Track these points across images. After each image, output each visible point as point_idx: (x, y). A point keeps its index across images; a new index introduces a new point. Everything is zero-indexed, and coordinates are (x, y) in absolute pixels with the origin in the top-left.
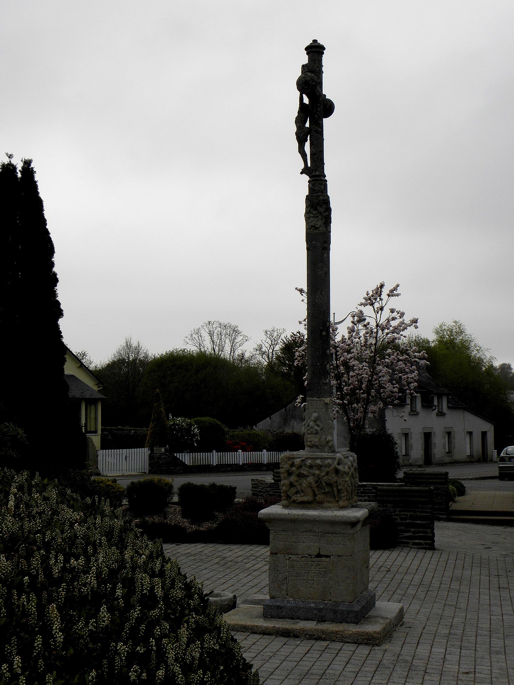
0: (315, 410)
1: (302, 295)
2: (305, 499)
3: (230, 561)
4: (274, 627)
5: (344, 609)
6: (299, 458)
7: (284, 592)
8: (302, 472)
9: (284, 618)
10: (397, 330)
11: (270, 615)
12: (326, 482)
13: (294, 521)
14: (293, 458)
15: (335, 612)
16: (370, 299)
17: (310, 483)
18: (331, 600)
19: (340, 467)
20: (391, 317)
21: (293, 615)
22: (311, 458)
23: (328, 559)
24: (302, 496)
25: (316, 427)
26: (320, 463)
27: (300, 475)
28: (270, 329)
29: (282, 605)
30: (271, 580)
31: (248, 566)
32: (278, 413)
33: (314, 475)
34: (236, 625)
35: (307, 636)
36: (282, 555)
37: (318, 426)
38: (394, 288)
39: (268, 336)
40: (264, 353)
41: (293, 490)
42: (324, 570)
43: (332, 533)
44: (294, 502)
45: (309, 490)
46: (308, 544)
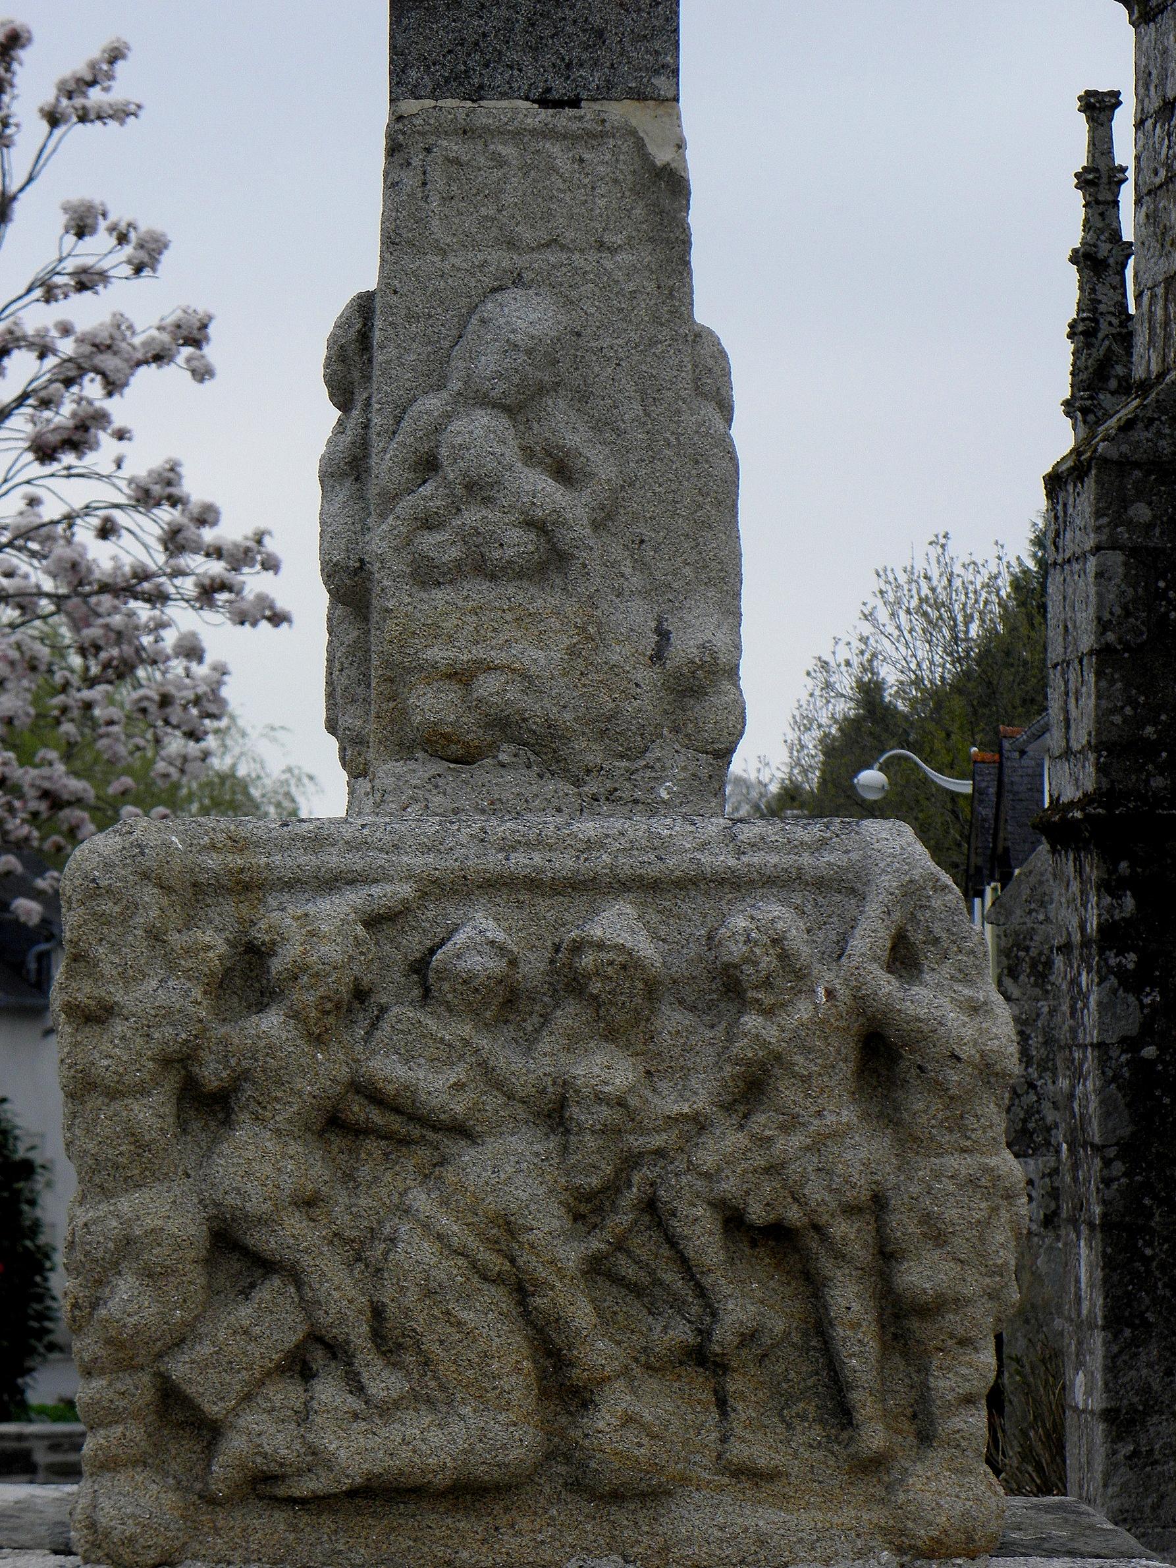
0: (501, 259)
2: (429, 1442)
6: (331, 883)
8: (389, 1069)
10: (108, 362)
12: (733, 1221)
14: (246, 887)
17: (507, 1229)
20: (70, 265)
22: (494, 885)
24: (386, 1410)
25: (538, 485)
26: (646, 948)
27: (358, 1122)
33: (554, 1112)
37: (564, 470)
38: (93, 66)
41: (264, 1322)
44: (263, 1486)
45: (490, 1324)
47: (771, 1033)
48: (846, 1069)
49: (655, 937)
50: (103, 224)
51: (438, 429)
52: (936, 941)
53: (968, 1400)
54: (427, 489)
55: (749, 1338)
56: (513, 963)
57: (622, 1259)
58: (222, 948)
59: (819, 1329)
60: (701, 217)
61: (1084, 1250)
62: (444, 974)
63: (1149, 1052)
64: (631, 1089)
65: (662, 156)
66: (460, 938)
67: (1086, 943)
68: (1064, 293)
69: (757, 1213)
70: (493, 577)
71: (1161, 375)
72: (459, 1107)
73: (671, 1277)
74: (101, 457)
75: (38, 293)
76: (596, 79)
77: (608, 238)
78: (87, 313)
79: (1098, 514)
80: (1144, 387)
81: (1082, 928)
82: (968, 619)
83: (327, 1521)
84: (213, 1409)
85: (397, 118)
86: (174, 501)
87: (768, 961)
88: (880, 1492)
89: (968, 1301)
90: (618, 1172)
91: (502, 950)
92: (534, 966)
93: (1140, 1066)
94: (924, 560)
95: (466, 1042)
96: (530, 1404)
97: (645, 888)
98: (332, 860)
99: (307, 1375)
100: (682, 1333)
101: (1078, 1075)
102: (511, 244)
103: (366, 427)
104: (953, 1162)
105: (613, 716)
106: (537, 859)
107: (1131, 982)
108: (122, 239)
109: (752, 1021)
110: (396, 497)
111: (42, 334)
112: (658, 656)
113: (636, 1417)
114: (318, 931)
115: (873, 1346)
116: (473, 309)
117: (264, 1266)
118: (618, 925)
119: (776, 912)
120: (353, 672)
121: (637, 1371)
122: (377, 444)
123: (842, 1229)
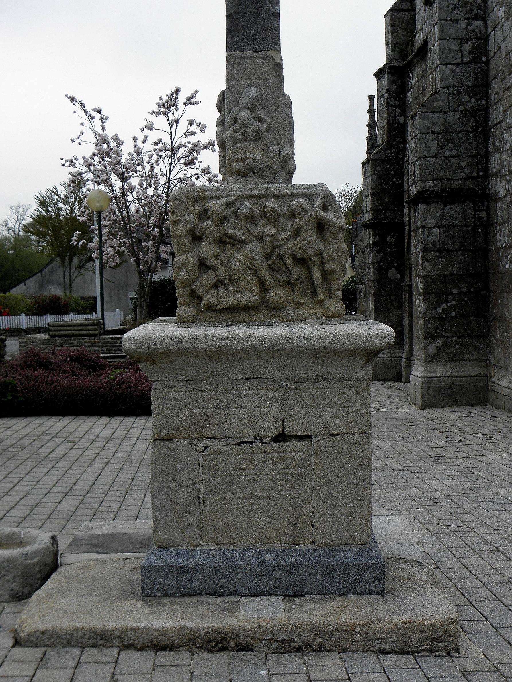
0: (248, 82)
1: (74, 104)
2: (240, 299)
3: (12, 446)
4: (183, 628)
5: (350, 562)
6: (219, 197)
7: (194, 532)
8: (231, 231)
9: (196, 594)
10: (197, 148)
11: (159, 590)
13: (219, 354)
15: (328, 571)
16: (164, 105)
17: (253, 260)
18: (314, 542)
19: (329, 216)
20: (189, 131)
21: (221, 587)
22: (249, 197)
23: (306, 444)
24: (232, 293)
25: (256, 124)
26: (277, 207)
27: (226, 242)
28: (15, 204)
29: (190, 564)
30: (158, 504)
31: (44, 451)
32: (33, 279)
33: (261, 238)
34: (77, 630)
35: (275, 645)
36: (187, 442)
37: (261, 121)
38: (192, 94)
39: (14, 211)
40: (10, 229)
41: (209, 278)
42: (294, 471)
43: (315, 381)
44: (210, 308)
45: (250, 277)
46: (254, 411)
47: (301, 222)
48: (315, 229)
49: (279, 206)
50: (195, 123)
51: (237, 114)
52: (331, 205)
53: (338, 289)
54: (236, 125)
55: (298, 279)
56: (253, 211)
57: (274, 265)
58: (199, 209)
59: (311, 277)
60: (286, 73)
61: (370, 299)
62: (240, 213)
63: (381, 264)
64: (275, 233)
65: (278, 61)
66: (243, 206)
67: (370, 245)
68: (365, 132)
69: (298, 256)
70: (248, 141)
71: (382, 144)
72: (244, 238)
73: (283, 268)
74: (196, 166)
75: (184, 136)
76: (265, 47)
77: (268, 77)
78: (193, 139)
79: (371, 169)
80: (379, 146)
81: (369, 242)
82: (352, 198)
83: (222, 314)
84: (201, 294)
85: (228, 55)
86: (209, 173)
87: (300, 209)
88: (322, 306)
89: (338, 271)
90: (273, 249)
91: (250, 208)
92: (257, 212)
93: (380, 267)
94: (344, 188)
95: (245, 226)
96: (258, 292)
97: (277, 197)
98: (219, 193)
99: (218, 288)
100: (286, 279)
101: (369, 269)
102: (250, 79)
103: (224, 115)
104: (334, 245)
105: (271, 166)
106: (257, 192)
107: (378, 252)
108: (198, 126)
109: (297, 220)
110: (230, 127)
111: (185, 143)
112: (279, 155)
113: (276, 294)
114: (216, 206)
115: (320, 280)
116: (243, 91)
117: (208, 268)
118: (272, 203)
119: (301, 200)
120: (224, 161)
121: (278, 286)
122: (226, 117)
123: (314, 258)
